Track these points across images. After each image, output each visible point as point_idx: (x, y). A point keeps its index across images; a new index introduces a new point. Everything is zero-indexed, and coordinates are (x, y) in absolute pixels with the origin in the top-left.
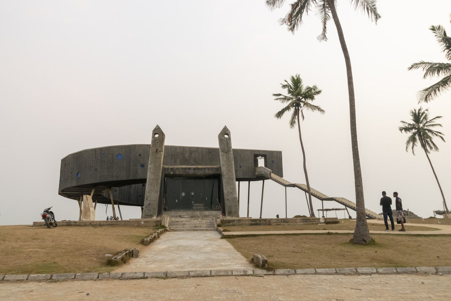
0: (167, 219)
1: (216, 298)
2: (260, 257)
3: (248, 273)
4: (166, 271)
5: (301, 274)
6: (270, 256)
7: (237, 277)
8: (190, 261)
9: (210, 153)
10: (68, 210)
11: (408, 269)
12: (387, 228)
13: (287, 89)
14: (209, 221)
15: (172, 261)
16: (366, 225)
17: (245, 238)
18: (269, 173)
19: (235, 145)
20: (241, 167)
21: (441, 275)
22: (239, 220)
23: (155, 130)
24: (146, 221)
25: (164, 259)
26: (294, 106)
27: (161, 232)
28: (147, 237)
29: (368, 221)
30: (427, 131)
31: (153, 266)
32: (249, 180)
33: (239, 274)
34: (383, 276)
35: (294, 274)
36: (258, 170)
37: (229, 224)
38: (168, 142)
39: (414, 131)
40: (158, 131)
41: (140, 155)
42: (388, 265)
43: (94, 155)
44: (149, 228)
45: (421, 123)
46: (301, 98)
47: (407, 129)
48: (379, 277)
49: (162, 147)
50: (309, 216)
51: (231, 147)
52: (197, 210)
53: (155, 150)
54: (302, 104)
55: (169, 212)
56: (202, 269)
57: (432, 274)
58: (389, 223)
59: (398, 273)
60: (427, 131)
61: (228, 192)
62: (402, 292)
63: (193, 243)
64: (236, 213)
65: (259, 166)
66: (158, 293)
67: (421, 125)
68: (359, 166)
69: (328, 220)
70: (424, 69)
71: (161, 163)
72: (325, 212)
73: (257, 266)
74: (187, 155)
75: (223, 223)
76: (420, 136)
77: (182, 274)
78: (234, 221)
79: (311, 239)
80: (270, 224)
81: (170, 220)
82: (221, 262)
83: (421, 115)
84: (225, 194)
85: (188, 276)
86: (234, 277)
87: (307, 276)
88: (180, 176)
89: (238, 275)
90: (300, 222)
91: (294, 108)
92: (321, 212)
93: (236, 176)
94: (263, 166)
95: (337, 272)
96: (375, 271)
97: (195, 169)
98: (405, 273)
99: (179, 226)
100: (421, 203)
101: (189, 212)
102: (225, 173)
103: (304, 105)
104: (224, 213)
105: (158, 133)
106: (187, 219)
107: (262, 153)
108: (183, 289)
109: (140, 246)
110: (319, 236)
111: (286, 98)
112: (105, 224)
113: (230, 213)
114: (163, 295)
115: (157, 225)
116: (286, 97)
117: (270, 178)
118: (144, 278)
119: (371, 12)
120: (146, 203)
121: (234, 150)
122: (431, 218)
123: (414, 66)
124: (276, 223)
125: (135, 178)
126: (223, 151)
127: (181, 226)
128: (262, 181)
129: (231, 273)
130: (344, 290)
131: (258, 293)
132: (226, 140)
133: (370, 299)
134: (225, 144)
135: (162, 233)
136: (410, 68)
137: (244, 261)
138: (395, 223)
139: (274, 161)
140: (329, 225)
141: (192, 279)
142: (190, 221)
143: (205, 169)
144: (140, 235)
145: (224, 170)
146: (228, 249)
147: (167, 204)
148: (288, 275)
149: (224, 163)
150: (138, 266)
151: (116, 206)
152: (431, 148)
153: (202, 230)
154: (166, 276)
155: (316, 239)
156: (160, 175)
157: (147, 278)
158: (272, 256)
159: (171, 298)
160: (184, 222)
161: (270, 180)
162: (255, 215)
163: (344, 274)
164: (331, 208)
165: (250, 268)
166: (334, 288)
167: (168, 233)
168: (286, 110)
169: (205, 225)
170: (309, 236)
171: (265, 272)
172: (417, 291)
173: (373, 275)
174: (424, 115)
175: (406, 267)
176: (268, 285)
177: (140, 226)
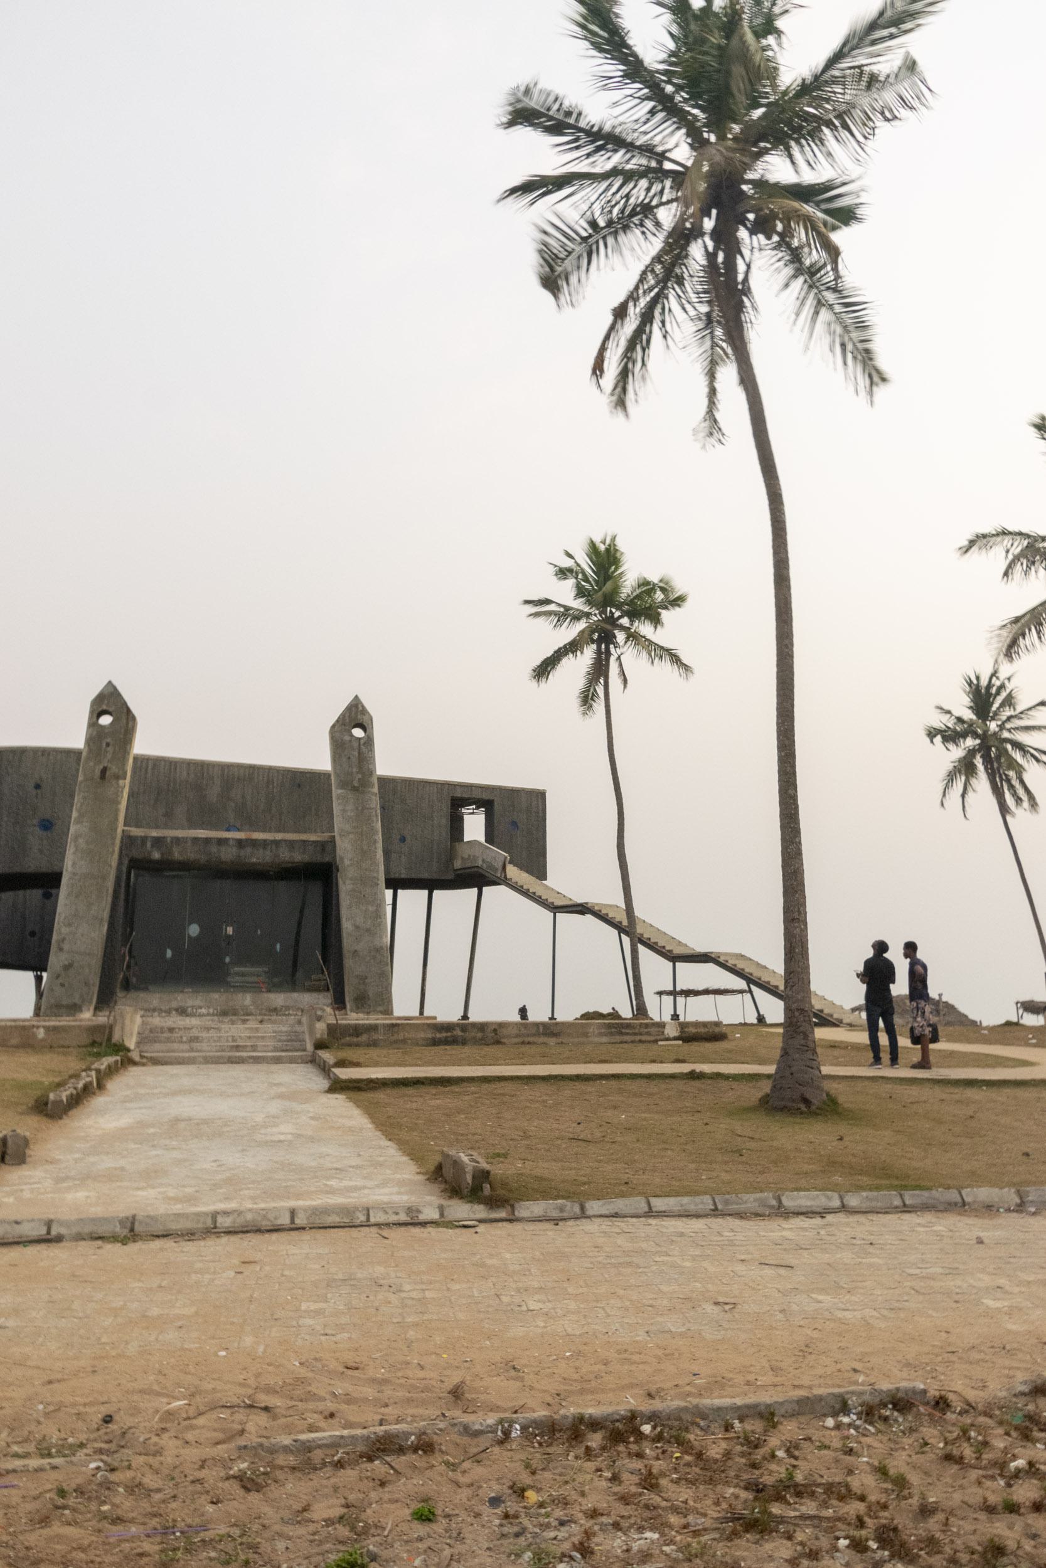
0: (133, 1021)
1: (313, 1306)
2: (465, 1159)
3: (422, 1217)
4: (129, 1213)
5: (601, 1216)
6: (498, 1155)
7: (385, 1233)
8: (219, 1177)
9: (298, 789)
11: (939, 1194)
12: (877, 1060)
13: (570, 582)
14: (284, 1029)
15: (150, 1176)
16: (809, 1048)
17: (410, 1091)
18: (499, 865)
19: (389, 762)
20: (403, 839)
21: (1034, 1214)
22: (393, 1025)
23: (100, 699)
24: (55, 1029)
25: (122, 1169)
26: (593, 641)
27: (109, 1066)
28: (59, 1085)
29: (821, 1033)
30: (1009, 747)
31: (81, 1195)
32: (431, 885)
33: (393, 1218)
34: (861, 1218)
35: (576, 1218)
36: (463, 851)
37: (355, 1039)
38: (147, 743)
39: (970, 742)
40: (110, 702)
41: (38, 787)
42: (877, 1182)
44: (64, 1054)
45: (993, 719)
46: (617, 614)
47: (950, 736)
48: (848, 1224)
49: (124, 764)
50: (630, 1015)
51: (371, 773)
52: (244, 988)
53: (98, 773)
54: (620, 637)
55: (142, 995)
56: (262, 1205)
57: (1008, 1210)
58: (883, 1039)
59: (906, 1209)
60: (1009, 747)
61: (357, 927)
62: (918, 1271)
63: (224, 1107)
64: (384, 1001)
65: (466, 839)
66: (100, 1296)
67: (993, 726)
68: (799, 853)
69: (693, 1030)
70: (1007, 551)
71: (116, 819)
72: (681, 1000)
73: (455, 1191)
74: (213, 793)
75: (336, 1037)
76: (987, 760)
77: (189, 1225)
78: (374, 1028)
79: (635, 1095)
80: (498, 1042)
81: (143, 1023)
82: (328, 1178)
83: (994, 690)
84: (344, 935)
85: (211, 1229)
86: (374, 1230)
87: (619, 1223)
88: (185, 866)
89: (387, 1225)
90: (601, 1035)
91: (594, 646)
92: (668, 1000)
93: (387, 872)
94: (481, 837)
95: (716, 1209)
96: (836, 1203)
97: (240, 843)
98: (925, 1207)
99: (176, 1046)
100: (981, 981)
101: (216, 996)
102: (347, 862)
103: (627, 639)
104: (339, 1002)
105: (112, 709)
106: (207, 1021)
107: (477, 795)
108: (194, 1277)
109: (33, 1121)
110: (663, 1085)
111: (566, 615)
113: (362, 1002)
114: (118, 1302)
115: (93, 1043)
116: (567, 608)
117: (505, 881)
118: (50, 1239)
119: (855, 358)
120: (56, 960)
121: (384, 781)
122: (1008, 1024)
123: (979, 541)
124: (517, 1036)
125: (17, 869)
126: (343, 785)
127: (186, 1047)
128: (475, 890)
129: (362, 1218)
130: (740, 1268)
131: (458, 1287)
132: (356, 745)
133: (820, 1297)
134: (354, 760)
135: (112, 1071)
136: (967, 550)
137: (409, 1171)
138: (904, 1042)
139: (519, 820)
140: (695, 1047)
141: (224, 1239)
142: (219, 1029)
143: (277, 843)
144: (31, 1077)
145: (345, 850)
146: (351, 1130)
147: (136, 960)
148: (556, 1221)
149: (347, 827)
150: (27, 1195)
152: (1019, 801)
153: (257, 1060)
154: (132, 1230)
155: (652, 1094)
156: (114, 862)
157: (59, 1239)
158: (505, 1156)
159: (149, 1314)
160: (195, 1033)
161: (502, 889)
162: (445, 1009)
163: (740, 1215)
164: (701, 989)
165: (428, 1198)
166: (706, 1264)
167: (134, 1070)
168: (566, 654)
169: (271, 1043)
170: (628, 1082)
171: (480, 1211)
172: (961, 1267)
173: (830, 1218)
174: (1004, 694)
175: (929, 1189)
176: (491, 1256)
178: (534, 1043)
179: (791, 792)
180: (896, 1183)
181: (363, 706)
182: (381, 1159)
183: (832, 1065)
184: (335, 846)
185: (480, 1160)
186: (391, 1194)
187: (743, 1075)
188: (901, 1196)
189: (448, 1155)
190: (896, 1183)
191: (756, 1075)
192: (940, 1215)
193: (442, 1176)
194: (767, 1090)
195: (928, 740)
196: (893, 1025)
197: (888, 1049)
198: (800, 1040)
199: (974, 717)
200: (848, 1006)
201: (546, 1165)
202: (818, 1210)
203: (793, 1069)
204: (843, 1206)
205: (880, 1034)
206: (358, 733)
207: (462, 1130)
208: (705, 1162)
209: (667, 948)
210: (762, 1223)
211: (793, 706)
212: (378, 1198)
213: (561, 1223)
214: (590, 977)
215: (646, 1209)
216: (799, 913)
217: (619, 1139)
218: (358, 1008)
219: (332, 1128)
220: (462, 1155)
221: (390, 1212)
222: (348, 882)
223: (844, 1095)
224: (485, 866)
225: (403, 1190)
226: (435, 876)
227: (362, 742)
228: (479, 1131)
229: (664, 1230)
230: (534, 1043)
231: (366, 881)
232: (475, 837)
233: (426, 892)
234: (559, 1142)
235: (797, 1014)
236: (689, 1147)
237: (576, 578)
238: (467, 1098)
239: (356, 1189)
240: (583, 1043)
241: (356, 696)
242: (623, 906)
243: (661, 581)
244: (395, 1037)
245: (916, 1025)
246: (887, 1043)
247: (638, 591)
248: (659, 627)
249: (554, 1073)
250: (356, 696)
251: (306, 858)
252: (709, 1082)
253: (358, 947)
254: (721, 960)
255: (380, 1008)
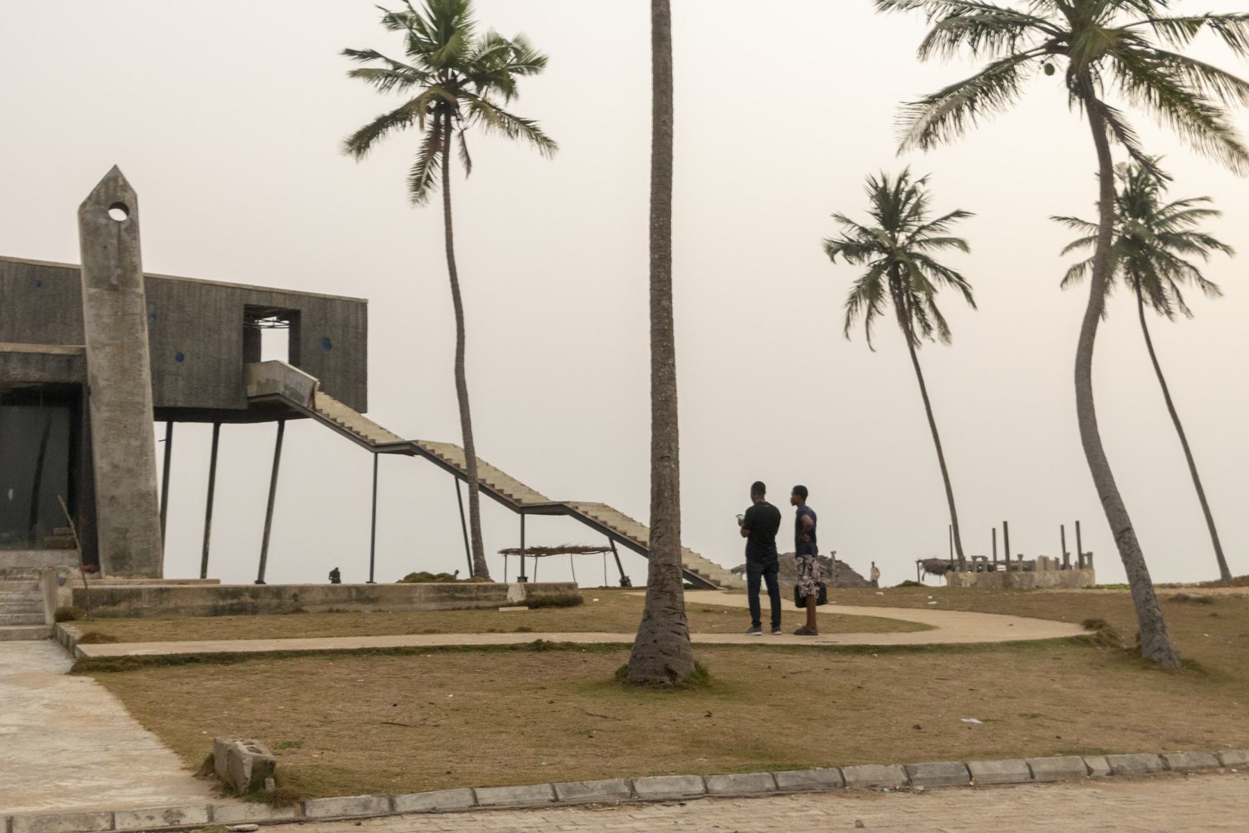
2: (242, 747)
6: (290, 745)
12: (757, 625)
13: (403, 33)
14: (15, 597)
16: (678, 610)
17: (181, 671)
18: (306, 392)
19: (157, 259)
20: (180, 358)
21: (922, 793)
22: (161, 591)
26: (430, 111)
30: (918, 263)
32: (217, 416)
36: (259, 374)
37: (111, 609)
39: (876, 257)
46: (461, 77)
47: (852, 250)
48: (710, 811)
51: (136, 267)
54: (464, 106)
57: (894, 790)
58: (765, 602)
59: (778, 792)
64: (152, 560)
67: (902, 238)
68: (672, 378)
72: (530, 560)
73: (229, 788)
75: (84, 606)
76: (894, 277)
80: (298, 611)
82: (61, 778)
83: (903, 197)
92: (515, 560)
95: (557, 800)
98: (803, 789)
102: (102, 383)
103: (474, 108)
104: (90, 562)
107: (279, 303)
110: (501, 658)
111: (396, 75)
113: (121, 562)
116: (397, 66)
121: (156, 284)
122: (908, 584)
124: (323, 602)
126: (97, 282)
128: (275, 424)
132: (114, 230)
137: (172, 767)
138: (788, 605)
139: (332, 338)
140: (543, 613)
145: (99, 365)
146: (98, 719)
148: (358, 821)
149: (103, 338)
152: (927, 328)
155: (487, 669)
161: (311, 423)
162: (234, 570)
163: (585, 806)
164: (554, 547)
165: (194, 798)
173: (690, 805)
174: (913, 201)
175: (806, 768)
178: (344, 611)
179: (664, 303)
180: (768, 762)
181: (124, 180)
182: (136, 753)
183: (705, 632)
184: (85, 362)
185: (262, 748)
186: (146, 795)
187: (599, 644)
188: (774, 777)
189: (222, 745)
190: (768, 762)
191: (613, 644)
192: (817, 797)
193: (214, 771)
194: (626, 661)
195: (828, 258)
196: (777, 585)
197: (770, 614)
198: (665, 602)
199: (881, 228)
200: (729, 565)
201: (349, 755)
202: (680, 796)
203: (657, 636)
204: (707, 791)
205: (761, 597)
206: (117, 215)
207: (244, 716)
208: (546, 746)
209: (515, 497)
210: (610, 814)
211: (670, 197)
212: (132, 799)
213: (364, 823)
214: (420, 531)
215: (471, 803)
216: (670, 450)
217: (444, 722)
218: (115, 569)
219: (71, 717)
220: (239, 743)
221: (143, 816)
222: (103, 408)
223: (716, 666)
224: (287, 393)
225: (161, 789)
226: (222, 406)
227: (123, 227)
228: (267, 717)
229: (492, 826)
230: (344, 611)
231: (128, 407)
232: (278, 357)
233: (210, 426)
234: (369, 727)
235: (663, 570)
236: (528, 729)
237: (411, 28)
238: (254, 678)
239: (99, 789)
240: (406, 611)
241: (115, 167)
242: (461, 444)
243: (516, 41)
244: (165, 605)
245: (802, 584)
246: (769, 607)
247: (488, 50)
248: (512, 99)
249: (368, 646)
250: (115, 167)
251: (47, 377)
252: (559, 653)
253: (118, 492)
254: (580, 511)
255: (145, 570)
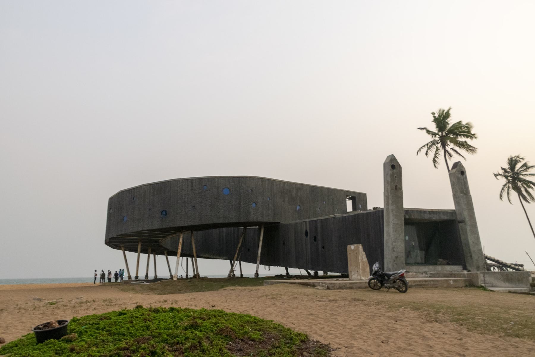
10: (115, 260)
43: (190, 187)
53: (394, 187)
112: (413, 284)
125: (247, 221)
151: (152, 256)
177: (450, 287)
